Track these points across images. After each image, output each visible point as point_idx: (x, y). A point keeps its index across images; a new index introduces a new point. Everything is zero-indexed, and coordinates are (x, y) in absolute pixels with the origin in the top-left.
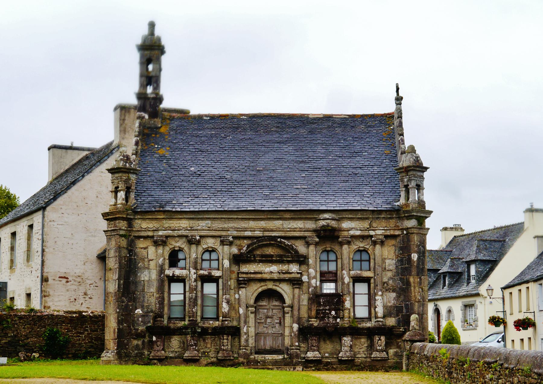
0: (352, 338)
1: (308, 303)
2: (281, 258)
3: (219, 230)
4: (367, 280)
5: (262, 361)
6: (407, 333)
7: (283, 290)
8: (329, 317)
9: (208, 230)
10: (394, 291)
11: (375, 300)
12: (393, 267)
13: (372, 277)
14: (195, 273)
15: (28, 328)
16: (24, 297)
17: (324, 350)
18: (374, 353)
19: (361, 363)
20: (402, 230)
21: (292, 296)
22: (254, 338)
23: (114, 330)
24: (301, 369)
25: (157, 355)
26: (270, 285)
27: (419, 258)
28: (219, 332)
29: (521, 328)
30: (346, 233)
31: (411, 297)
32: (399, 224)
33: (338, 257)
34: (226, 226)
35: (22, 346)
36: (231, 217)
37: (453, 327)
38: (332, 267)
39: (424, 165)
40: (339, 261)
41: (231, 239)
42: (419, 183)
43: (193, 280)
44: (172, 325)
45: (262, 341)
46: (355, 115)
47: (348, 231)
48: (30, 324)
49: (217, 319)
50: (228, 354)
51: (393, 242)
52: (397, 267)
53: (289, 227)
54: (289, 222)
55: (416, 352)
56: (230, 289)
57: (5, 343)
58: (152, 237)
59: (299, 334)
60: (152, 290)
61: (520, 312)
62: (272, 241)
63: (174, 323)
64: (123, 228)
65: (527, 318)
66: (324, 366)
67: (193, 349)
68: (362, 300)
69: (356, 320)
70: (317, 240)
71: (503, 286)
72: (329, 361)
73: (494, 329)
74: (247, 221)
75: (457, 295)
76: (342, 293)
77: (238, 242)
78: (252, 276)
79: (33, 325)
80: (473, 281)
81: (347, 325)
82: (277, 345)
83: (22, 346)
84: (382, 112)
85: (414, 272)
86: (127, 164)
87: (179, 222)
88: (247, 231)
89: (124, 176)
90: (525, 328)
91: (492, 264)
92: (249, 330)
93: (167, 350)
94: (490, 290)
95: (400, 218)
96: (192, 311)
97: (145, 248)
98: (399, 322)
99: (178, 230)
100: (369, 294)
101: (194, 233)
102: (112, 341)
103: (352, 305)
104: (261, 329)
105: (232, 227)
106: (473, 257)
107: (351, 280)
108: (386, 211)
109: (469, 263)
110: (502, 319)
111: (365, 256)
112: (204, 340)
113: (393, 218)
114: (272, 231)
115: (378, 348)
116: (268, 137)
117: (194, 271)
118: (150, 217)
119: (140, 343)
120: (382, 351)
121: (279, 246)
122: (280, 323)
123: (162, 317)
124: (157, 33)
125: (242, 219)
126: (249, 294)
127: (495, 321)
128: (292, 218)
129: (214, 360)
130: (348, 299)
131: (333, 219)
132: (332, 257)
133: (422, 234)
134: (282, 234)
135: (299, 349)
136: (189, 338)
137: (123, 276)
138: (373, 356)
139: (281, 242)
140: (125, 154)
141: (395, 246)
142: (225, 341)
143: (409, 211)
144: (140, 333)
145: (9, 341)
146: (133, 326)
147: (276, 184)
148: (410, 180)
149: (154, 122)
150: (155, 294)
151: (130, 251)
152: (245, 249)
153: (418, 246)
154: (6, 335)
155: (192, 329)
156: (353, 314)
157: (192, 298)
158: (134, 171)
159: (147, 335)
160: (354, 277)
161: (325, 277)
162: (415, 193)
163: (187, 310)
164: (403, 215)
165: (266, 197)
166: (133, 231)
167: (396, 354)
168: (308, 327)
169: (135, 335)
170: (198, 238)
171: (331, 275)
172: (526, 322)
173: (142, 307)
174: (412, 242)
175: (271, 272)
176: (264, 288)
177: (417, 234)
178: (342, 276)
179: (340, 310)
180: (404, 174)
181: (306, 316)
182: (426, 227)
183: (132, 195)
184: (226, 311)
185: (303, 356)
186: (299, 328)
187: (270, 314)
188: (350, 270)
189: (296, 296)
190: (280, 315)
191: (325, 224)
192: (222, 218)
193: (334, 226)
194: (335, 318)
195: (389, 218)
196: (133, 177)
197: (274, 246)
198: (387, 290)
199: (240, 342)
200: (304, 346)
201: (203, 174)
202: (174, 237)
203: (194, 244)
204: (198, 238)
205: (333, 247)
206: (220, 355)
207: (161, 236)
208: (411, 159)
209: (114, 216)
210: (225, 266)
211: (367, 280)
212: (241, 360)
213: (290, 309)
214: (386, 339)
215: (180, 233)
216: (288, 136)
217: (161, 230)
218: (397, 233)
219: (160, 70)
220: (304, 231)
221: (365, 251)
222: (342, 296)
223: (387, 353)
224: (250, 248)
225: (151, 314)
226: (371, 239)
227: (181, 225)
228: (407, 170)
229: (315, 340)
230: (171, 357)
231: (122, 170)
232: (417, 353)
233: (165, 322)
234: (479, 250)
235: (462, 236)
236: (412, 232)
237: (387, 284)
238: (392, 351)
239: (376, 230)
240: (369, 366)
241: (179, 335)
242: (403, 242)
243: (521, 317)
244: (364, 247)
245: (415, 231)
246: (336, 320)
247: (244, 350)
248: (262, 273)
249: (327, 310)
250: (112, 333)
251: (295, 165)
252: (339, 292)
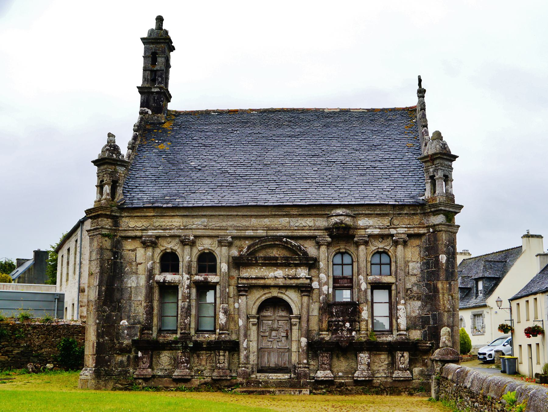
0: (370, 354)
1: (319, 314)
2: (287, 260)
3: (216, 229)
4: (387, 287)
5: (264, 382)
6: (437, 351)
7: (291, 299)
8: (342, 330)
9: (204, 229)
10: (419, 299)
11: (397, 309)
12: (417, 271)
13: (393, 283)
14: (188, 279)
15: (42, 338)
16: (71, 305)
17: (337, 369)
18: (396, 372)
19: (381, 384)
20: (428, 227)
21: (300, 306)
22: (256, 354)
23: (94, 344)
24: (308, 392)
25: (142, 373)
26: (275, 293)
27: (448, 260)
28: (215, 347)
29: (531, 335)
30: (362, 232)
31: (439, 305)
32: (424, 221)
33: (354, 260)
34: (224, 224)
35: (35, 356)
36: (230, 214)
37: (465, 333)
38: (347, 271)
39: (452, 153)
40: (355, 264)
41: (229, 239)
43: (186, 286)
44: (161, 339)
45: (266, 358)
46: (374, 109)
47: (366, 229)
48: (44, 334)
49: (214, 332)
50: (225, 373)
51: (417, 242)
52: (422, 271)
53: (297, 225)
54: (297, 219)
55: (450, 377)
56: (229, 297)
57: (17, 353)
58: (141, 237)
59: (308, 350)
60: (139, 298)
61: (528, 320)
62: (277, 241)
63: (165, 337)
64: (107, 227)
65: (536, 326)
66: (337, 387)
67: (184, 366)
68: (381, 311)
69: (375, 333)
70: (329, 240)
71: (510, 298)
72: (343, 381)
73: (502, 334)
74: (249, 219)
75: (468, 306)
76: (358, 301)
77: (237, 243)
78: (253, 281)
79: (47, 335)
80: (481, 295)
81: (364, 340)
82: (283, 361)
83: (35, 356)
84: (404, 106)
85: (442, 276)
86: (114, 155)
87: (171, 220)
88: (248, 230)
89: (110, 169)
90: (535, 335)
91: (496, 281)
92: (250, 345)
93: (155, 367)
94: (499, 301)
95: (426, 214)
96: (184, 322)
97: (133, 250)
98: (425, 335)
99: (170, 229)
100: (390, 302)
101: (187, 232)
102: (91, 357)
103: (370, 316)
104: (265, 344)
105: (231, 226)
106: (481, 275)
107: (369, 287)
108: (409, 206)
109: (477, 280)
110: (510, 326)
111: (385, 259)
112: (198, 356)
113: (417, 214)
114: (277, 229)
115: (401, 366)
116: (280, 131)
117: (187, 276)
118: (139, 214)
119: (125, 359)
120: (405, 369)
121: (285, 247)
122: (287, 337)
123: (150, 328)
124: (165, 26)
125: (243, 216)
126: (251, 303)
127: (504, 328)
128: (300, 215)
129: (209, 379)
130: (365, 308)
131: (347, 215)
132: (347, 259)
133: (452, 232)
134: (289, 233)
135: (308, 368)
136: (180, 354)
137: (105, 282)
138: (394, 376)
139: (286, 242)
140: (112, 144)
141: (420, 247)
142: (221, 357)
143: (436, 204)
144: (124, 348)
145: (22, 351)
146: (117, 340)
147: (284, 178)
148: (436, 170)
149: (158, 117)
150: (143, 303)
151: (115, 254)
152: (245, 250)
153: (447, 246)
154: (18, 346)
155: (183, 344)
156: (371, 326)
157: (184, 307)
158: (123, 163)
159: (126, 351)
160: (372, 283)
161: (339, 283)
162: (443, 185)
163: (179, 321)
164: (429, 210)
165: (272, 192)
166: (119, 230)
167: (422, 373)
168: (318, 341)
169: (119, 350)
170: (192, 238)
171: (346, 281)
172: (535, 330)
173: (129, 318)
174: (439, 241)
175: (276, 278)
176: (268, 296)
177: (445, 231)
178: (359, 282)
179: (355, 321)
180: (429, 164)
181: (316, 328)
183: (120, 191)
184: (223, 322)
185: (312, 375)
186: (308, 343)
187: (275, 326)
188: (367, 275)
189: (305, 305)
190: (287, 327)
191: (338, 221)
192: (219, 215)
193: (349, 223)
194: (350, 331)
195: (413, 214)
196: (121, 170)
197: (280, 247)
198: (410, 298)
199: (239, 359)
200: (314, 363)
201: (203, 169)
202: (165, 237)
203: (187, 245)
204: (192, 238)
205: (348, 248)
206: (215, 374)
207: (151, 236)
208: (438, 146)
209: (96, 213)
210: (223, 270)
211: (387, 287)
212: (240, 380)
213: (298, 320)
214: (410, 355)
215: (172, 232)
216: (301, 130)
217: (150, 229)
218: (422, 231)
220: (314, 230)
221: (385, 252)
222: (358, 305)
223: (412, 372)
224: (251, 250)
225: (139, 326)
227: (174, 224)
228: (432, 158)
229: (326, 357)
230: (159, 376)
231: (107, 161)
232: (452, 381)
233: (155, 335)
234: (485, 269)
235: (470, 259)
236: (440, 229)
237: (411, 291)
238: (416, 370)
239: (398, 228)
240: (390, 387)
241: (169, 350)
242: (429, 242)
243: (531, 324)
244: (383, 248)
245: (443, 228)
246: (351, 333)
247: (243, 369)
248: (265, 279)
249: (340, 321)
250: (91, 348)
251: (307, 158)
252: (355, 300)
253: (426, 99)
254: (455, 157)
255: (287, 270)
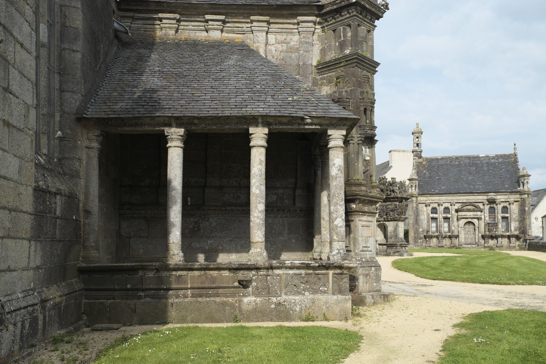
26: (470, 220)
51: (517, 203)
62: (471, 204)
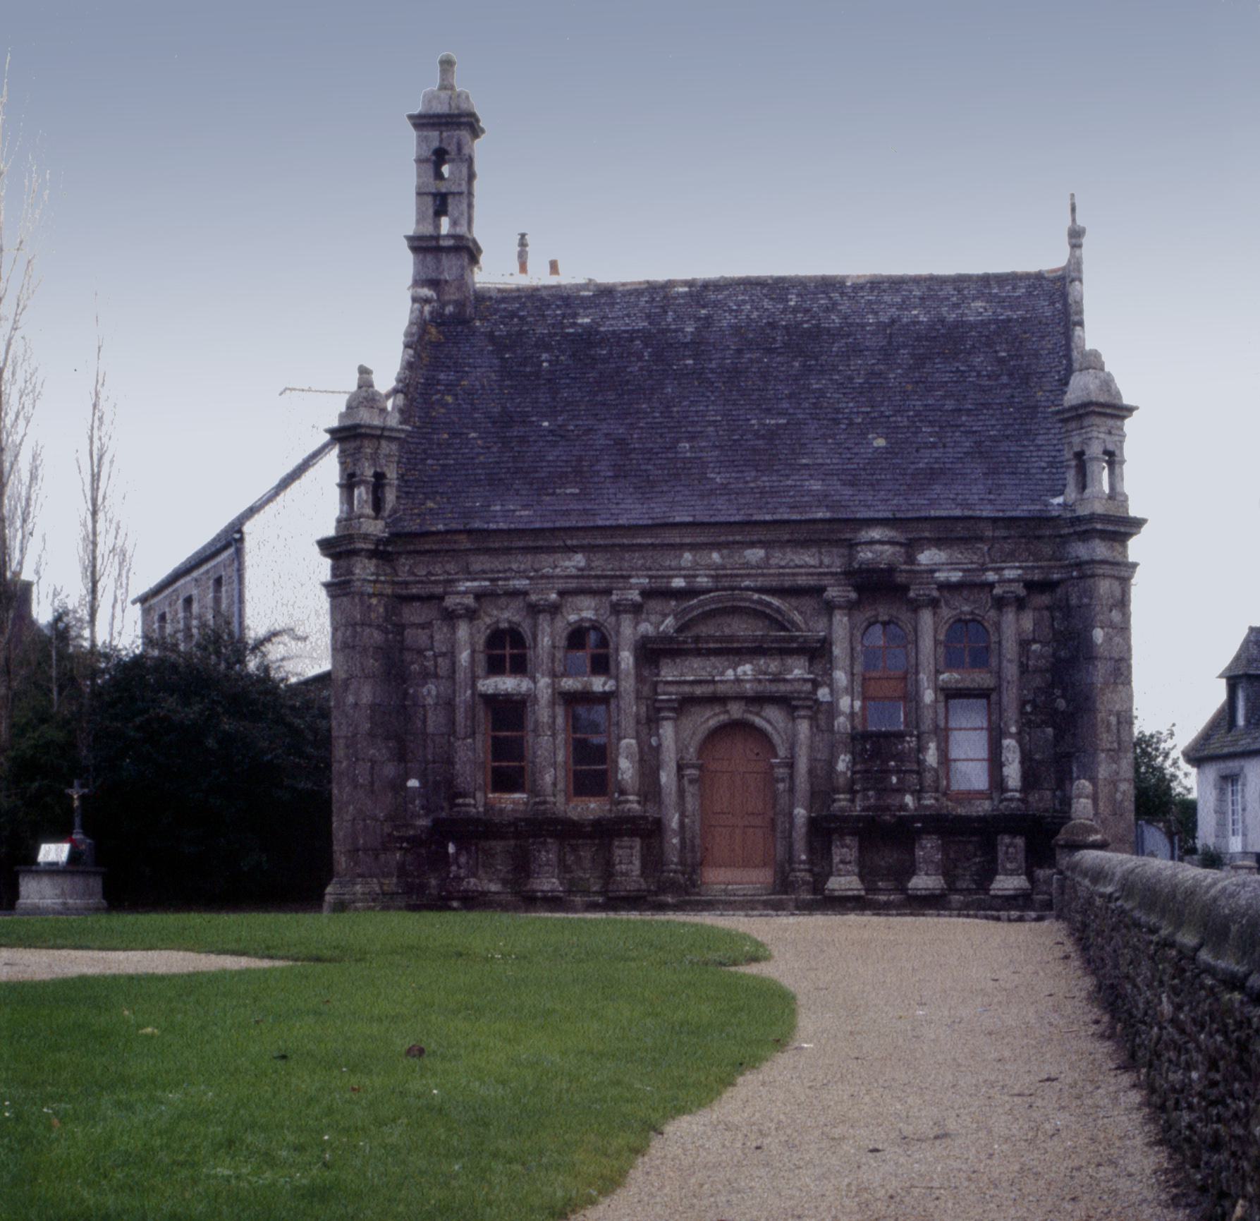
26: (736, 711)
42: (1110, 447)
107: (941, 698)
182: (1131, 559)
192: (613, 545)
219: (471, 176)
226: (991, 591)
253: (1086, 253)
254: (1130, 410)
255: (762, 662)
